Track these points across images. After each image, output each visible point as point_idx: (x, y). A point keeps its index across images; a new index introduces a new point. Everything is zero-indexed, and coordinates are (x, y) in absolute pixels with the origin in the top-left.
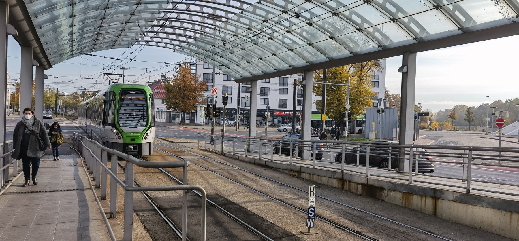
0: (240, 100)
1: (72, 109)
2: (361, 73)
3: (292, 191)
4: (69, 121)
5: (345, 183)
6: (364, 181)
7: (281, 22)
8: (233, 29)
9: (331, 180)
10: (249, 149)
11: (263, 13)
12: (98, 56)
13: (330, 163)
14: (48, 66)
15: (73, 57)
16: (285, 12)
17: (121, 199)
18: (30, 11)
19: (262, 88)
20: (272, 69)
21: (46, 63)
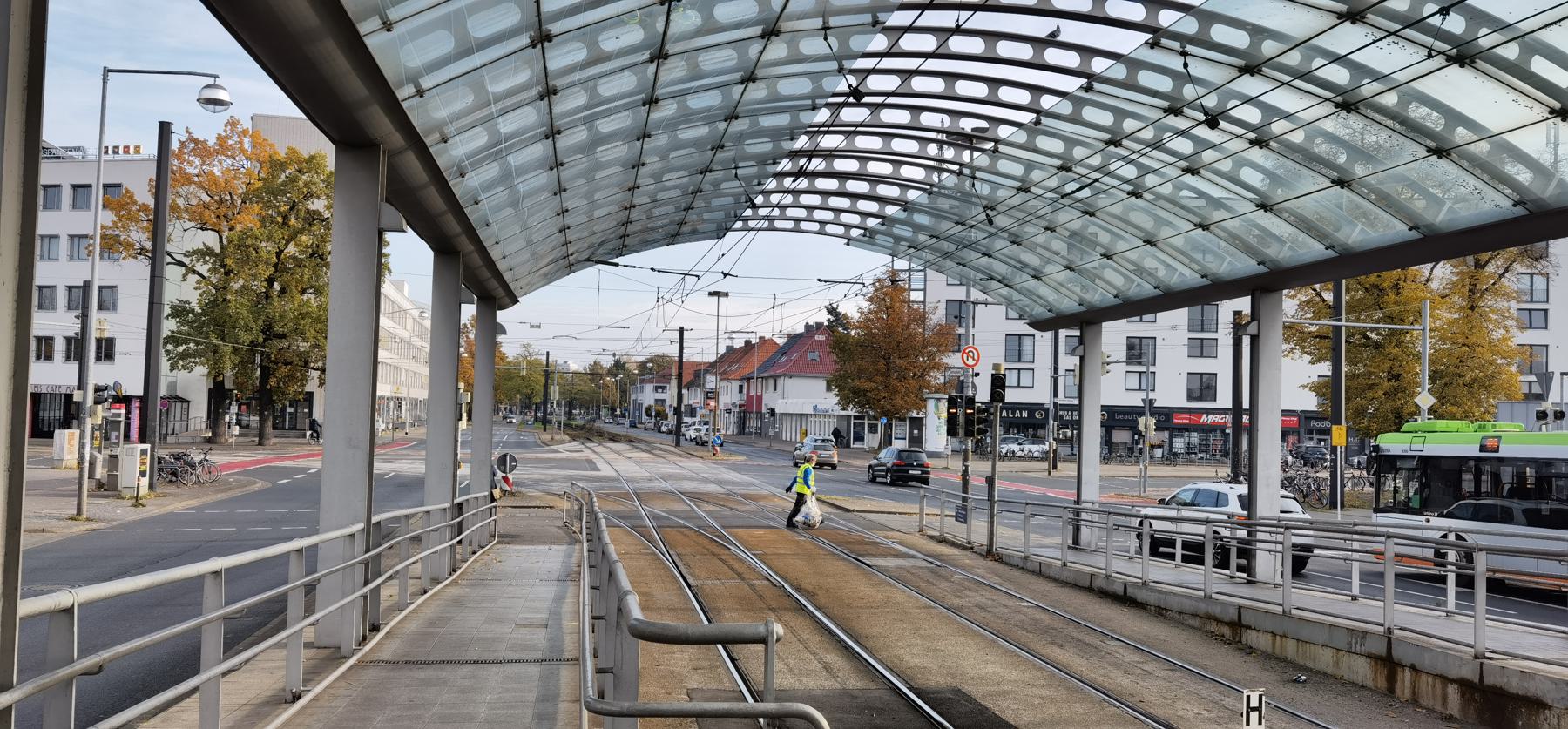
0: (1061, 381)
1: (588, 409)
2: (1475, 285)
3: (1207, 690)
4: (575, 443)
5: (1399, 677)
6: (1469, 672)
7: (1164, 141)
8: (1018, 170)
9: (1346, 659)
10: (1076, 540)
11: (1106, 119)
12: (635, 267)
13: (1350, 598)
14: (507, 300)
15: (571, 272)
16: (1174, 111)
17: (670, 691)
18: (441, 162)
19: (1134, 340)
20: (1187, 272)
21: (500, 292)
